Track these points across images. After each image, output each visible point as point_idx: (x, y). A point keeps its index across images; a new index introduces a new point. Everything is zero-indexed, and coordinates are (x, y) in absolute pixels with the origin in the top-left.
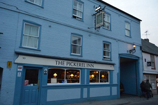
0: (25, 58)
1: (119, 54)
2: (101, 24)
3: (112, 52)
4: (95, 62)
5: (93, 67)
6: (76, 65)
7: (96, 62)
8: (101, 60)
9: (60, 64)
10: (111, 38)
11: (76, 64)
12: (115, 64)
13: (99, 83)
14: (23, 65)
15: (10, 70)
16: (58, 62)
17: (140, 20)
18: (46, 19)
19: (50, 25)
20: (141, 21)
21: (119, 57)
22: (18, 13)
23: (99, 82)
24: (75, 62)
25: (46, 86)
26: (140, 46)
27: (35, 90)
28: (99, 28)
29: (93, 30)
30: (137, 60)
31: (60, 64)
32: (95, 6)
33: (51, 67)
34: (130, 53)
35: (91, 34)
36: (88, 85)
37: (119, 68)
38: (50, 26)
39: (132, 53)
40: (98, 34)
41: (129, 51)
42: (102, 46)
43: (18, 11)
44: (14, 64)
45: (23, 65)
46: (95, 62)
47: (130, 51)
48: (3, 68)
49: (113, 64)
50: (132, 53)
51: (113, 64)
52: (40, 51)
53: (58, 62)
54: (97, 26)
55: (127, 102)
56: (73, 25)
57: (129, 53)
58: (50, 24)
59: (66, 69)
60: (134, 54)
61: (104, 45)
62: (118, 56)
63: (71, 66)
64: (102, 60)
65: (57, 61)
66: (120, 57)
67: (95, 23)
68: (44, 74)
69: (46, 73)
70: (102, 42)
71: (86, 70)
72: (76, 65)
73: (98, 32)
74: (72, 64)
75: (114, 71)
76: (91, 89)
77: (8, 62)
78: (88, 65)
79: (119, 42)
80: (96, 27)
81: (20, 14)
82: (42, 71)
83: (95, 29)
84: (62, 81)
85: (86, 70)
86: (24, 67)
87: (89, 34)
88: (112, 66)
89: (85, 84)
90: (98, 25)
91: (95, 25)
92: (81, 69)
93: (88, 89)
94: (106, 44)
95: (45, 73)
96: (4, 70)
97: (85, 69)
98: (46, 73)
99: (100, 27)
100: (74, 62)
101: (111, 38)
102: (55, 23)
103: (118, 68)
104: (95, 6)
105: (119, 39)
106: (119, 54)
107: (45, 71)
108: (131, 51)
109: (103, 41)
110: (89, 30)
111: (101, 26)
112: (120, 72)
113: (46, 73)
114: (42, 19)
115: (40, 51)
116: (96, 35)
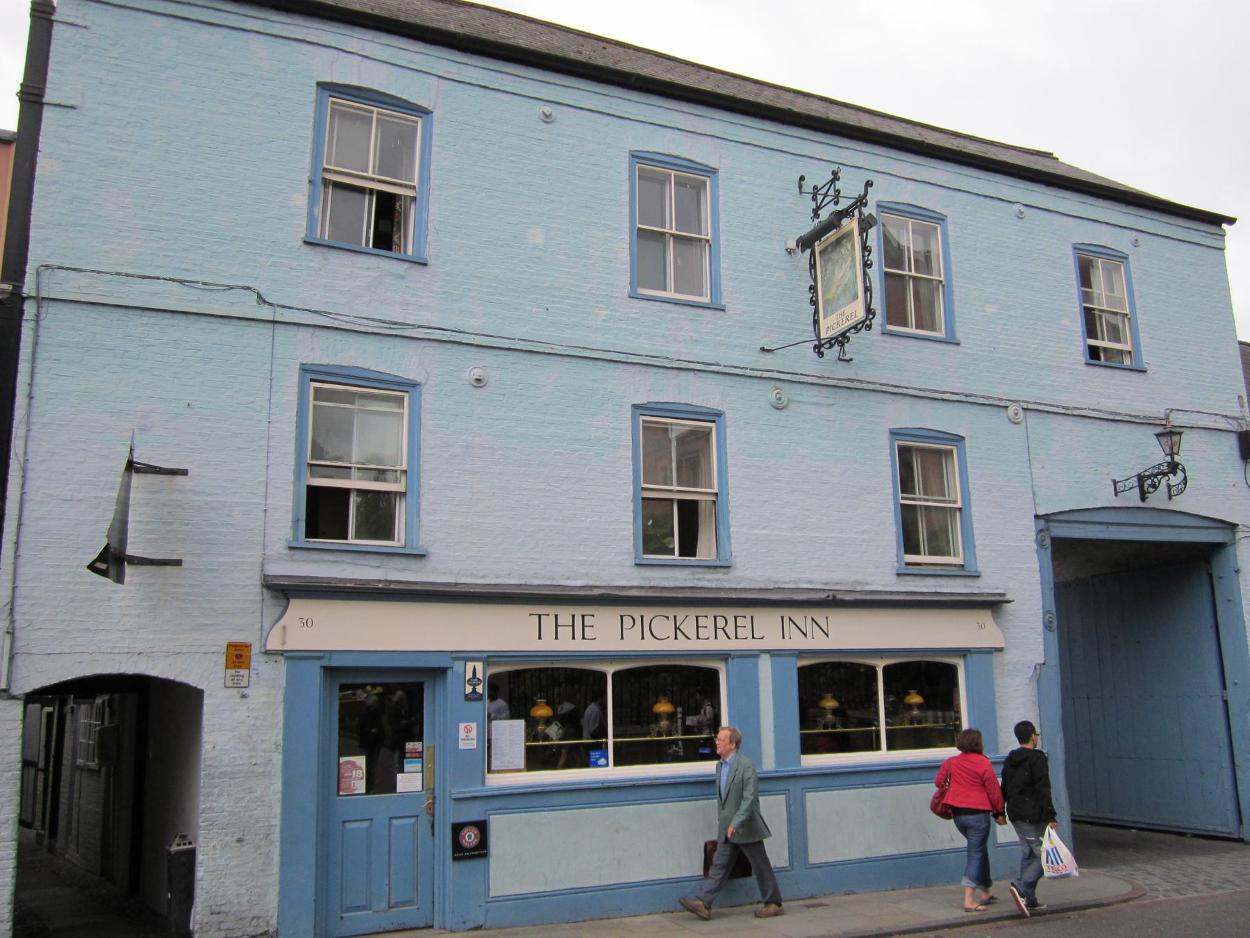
0: (983, 627)
1: (1037, 517)
2: (849, 310)
3: (976, 510)
4: (832, 602)
5: (828, 636)
6: (693, 634)
7: (839, 597)
8: (884, 581)
9: (565, 633)
10: (965, 401)
11: (689, 627)
12: (1008, 597)
13: (608, 772)
14: (321, 658)
15: (244, 696)
16: (548, 623)
17: (1216, 221)
18: (447, 336)
19: (477, 373)
20: (1231, 221)
21: (1041, 544)
22: (271, 326)
23: (878, 748)
24: (681, 613)
25: (475, 790)
26: (1234, 426)
27: (412, 820)
28: (842, 345)
29: (805, 362)
30: (1217, 548)
31: (565, 633)
32: (802, 178)
33: (506, 663)
34: (1143, 498)
35: (788, 392)
36: (789, 769)
37: (1047, 627)
38: (478, 380)
39: (1157, 499)
40: (851, 387)
41: (1134, 482)
42: (885, 469)
43: (266, 313)
44: (263, 658)
45: (321, 658)
46: (832, 602)
47: (1141, 478)
48: (201, 692)
49: (993, 605)
50: (1157, 499)
51: (993, 605)
52: (422, 556)
53: (548, 623)
54: (830, 326)
55: (1123, 888)
56: (643, 345)
57: (1133, 499)
58: (478, 364)
59: (610, 670)
60: (1179, 504)
61: (905, 457)
62: (1032, 535)
63: (650, 645)
64: (894, 578)
65: (540, 616)
66: (1048, 542)
67: (814, 302)
68: (467, 698)
69: (474, 690)
70: (885, 440)
71: (765, 664)
72: (692, 633)
73: (843, 372)
74: (663, 627)
75: (1007, 657)
76: (818, 802)
77: (230, 645)
78: (787, 620)
79: (1032, 419)
80: (819, 338)
81: (280, 330)
82: (445, 690)
83: (818, 349)
84: (594, 755)
85: (765, 664)
86: (330, 671)
87: (769, 392)
88: (985, 616)
89: (769, 764)
90: (832, 319)
91: (816, 322)
92: (725, 656)
93: (788, 806)
94: (922, 451)
95: (469, 689)
96: (206, 701)
97: (754, 655)
98: (474, 690)
99: (843, 335)
100: (671, 612)
101: (965, 401)
102: (513, 356)
103: (1040, 628)
104: (802, 178)
105: (1029, 395)
106: (1037, 517)
107: (469, 675)
108: (1145, 483)
109: (894, 433)
110: (768, 361)
111: (855, 327)
112: (1055, 661)
113: (479, 689)
114: (423, 344)
115: (422, 556)
116: (826, 392)
